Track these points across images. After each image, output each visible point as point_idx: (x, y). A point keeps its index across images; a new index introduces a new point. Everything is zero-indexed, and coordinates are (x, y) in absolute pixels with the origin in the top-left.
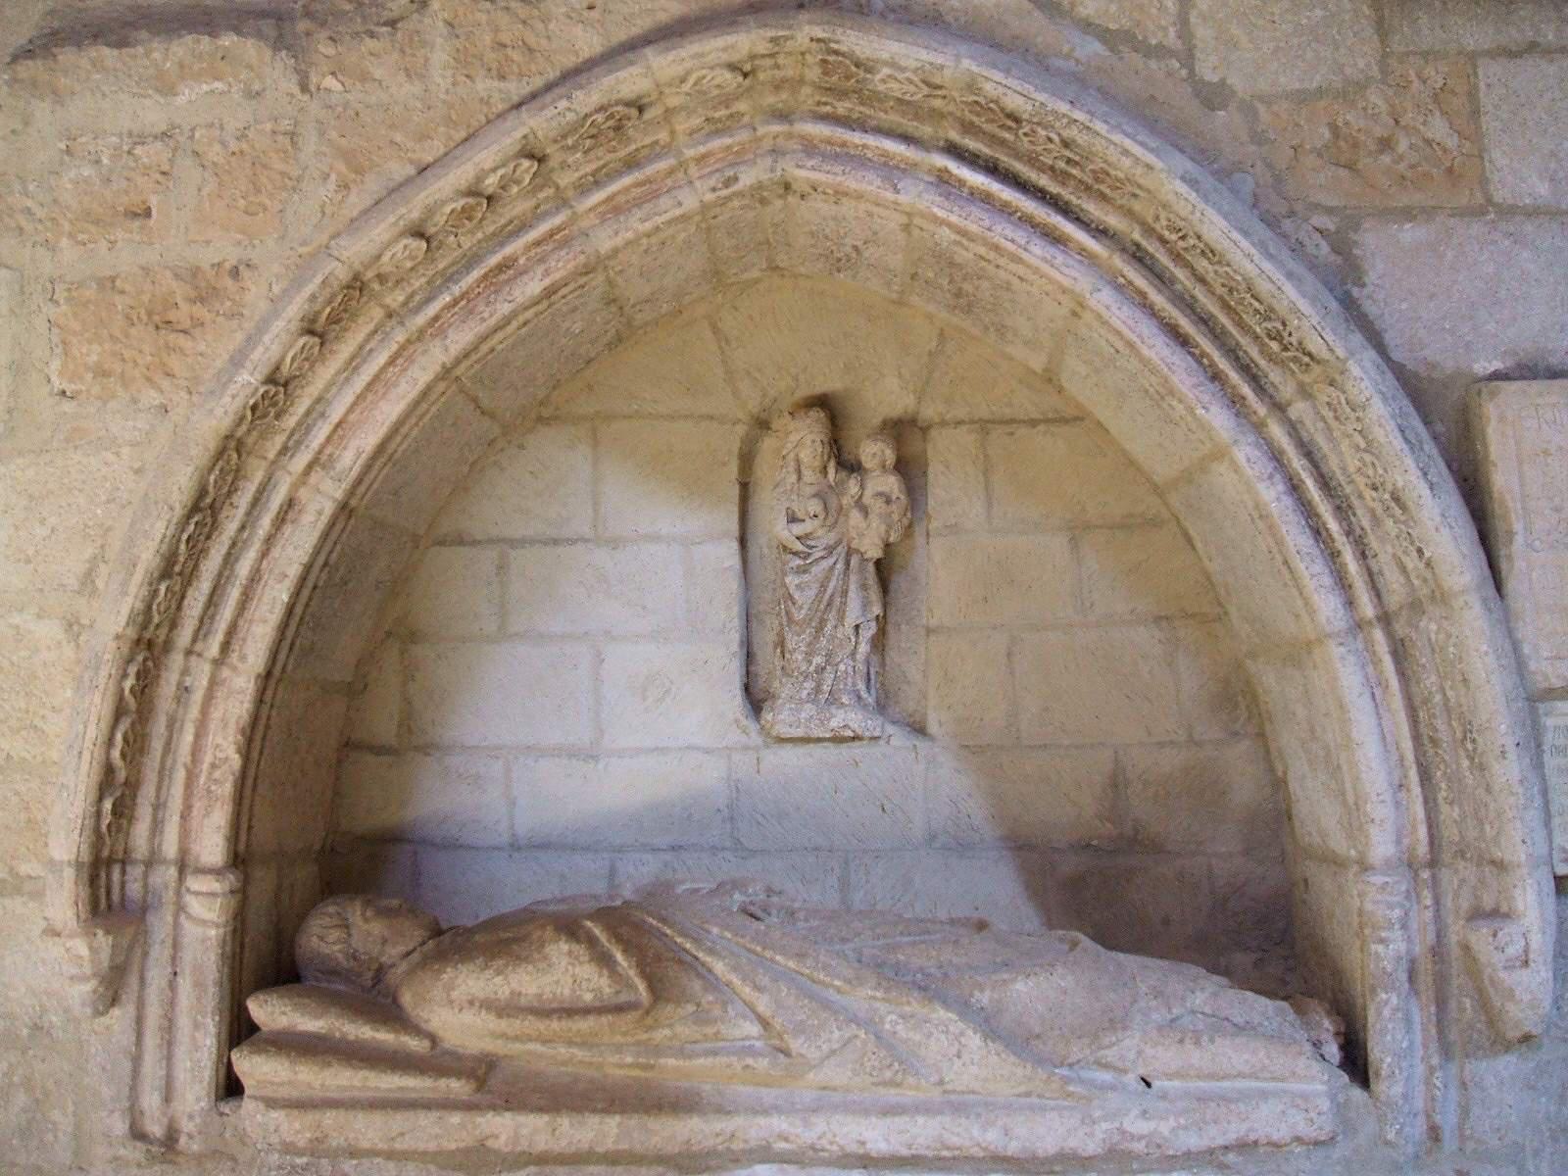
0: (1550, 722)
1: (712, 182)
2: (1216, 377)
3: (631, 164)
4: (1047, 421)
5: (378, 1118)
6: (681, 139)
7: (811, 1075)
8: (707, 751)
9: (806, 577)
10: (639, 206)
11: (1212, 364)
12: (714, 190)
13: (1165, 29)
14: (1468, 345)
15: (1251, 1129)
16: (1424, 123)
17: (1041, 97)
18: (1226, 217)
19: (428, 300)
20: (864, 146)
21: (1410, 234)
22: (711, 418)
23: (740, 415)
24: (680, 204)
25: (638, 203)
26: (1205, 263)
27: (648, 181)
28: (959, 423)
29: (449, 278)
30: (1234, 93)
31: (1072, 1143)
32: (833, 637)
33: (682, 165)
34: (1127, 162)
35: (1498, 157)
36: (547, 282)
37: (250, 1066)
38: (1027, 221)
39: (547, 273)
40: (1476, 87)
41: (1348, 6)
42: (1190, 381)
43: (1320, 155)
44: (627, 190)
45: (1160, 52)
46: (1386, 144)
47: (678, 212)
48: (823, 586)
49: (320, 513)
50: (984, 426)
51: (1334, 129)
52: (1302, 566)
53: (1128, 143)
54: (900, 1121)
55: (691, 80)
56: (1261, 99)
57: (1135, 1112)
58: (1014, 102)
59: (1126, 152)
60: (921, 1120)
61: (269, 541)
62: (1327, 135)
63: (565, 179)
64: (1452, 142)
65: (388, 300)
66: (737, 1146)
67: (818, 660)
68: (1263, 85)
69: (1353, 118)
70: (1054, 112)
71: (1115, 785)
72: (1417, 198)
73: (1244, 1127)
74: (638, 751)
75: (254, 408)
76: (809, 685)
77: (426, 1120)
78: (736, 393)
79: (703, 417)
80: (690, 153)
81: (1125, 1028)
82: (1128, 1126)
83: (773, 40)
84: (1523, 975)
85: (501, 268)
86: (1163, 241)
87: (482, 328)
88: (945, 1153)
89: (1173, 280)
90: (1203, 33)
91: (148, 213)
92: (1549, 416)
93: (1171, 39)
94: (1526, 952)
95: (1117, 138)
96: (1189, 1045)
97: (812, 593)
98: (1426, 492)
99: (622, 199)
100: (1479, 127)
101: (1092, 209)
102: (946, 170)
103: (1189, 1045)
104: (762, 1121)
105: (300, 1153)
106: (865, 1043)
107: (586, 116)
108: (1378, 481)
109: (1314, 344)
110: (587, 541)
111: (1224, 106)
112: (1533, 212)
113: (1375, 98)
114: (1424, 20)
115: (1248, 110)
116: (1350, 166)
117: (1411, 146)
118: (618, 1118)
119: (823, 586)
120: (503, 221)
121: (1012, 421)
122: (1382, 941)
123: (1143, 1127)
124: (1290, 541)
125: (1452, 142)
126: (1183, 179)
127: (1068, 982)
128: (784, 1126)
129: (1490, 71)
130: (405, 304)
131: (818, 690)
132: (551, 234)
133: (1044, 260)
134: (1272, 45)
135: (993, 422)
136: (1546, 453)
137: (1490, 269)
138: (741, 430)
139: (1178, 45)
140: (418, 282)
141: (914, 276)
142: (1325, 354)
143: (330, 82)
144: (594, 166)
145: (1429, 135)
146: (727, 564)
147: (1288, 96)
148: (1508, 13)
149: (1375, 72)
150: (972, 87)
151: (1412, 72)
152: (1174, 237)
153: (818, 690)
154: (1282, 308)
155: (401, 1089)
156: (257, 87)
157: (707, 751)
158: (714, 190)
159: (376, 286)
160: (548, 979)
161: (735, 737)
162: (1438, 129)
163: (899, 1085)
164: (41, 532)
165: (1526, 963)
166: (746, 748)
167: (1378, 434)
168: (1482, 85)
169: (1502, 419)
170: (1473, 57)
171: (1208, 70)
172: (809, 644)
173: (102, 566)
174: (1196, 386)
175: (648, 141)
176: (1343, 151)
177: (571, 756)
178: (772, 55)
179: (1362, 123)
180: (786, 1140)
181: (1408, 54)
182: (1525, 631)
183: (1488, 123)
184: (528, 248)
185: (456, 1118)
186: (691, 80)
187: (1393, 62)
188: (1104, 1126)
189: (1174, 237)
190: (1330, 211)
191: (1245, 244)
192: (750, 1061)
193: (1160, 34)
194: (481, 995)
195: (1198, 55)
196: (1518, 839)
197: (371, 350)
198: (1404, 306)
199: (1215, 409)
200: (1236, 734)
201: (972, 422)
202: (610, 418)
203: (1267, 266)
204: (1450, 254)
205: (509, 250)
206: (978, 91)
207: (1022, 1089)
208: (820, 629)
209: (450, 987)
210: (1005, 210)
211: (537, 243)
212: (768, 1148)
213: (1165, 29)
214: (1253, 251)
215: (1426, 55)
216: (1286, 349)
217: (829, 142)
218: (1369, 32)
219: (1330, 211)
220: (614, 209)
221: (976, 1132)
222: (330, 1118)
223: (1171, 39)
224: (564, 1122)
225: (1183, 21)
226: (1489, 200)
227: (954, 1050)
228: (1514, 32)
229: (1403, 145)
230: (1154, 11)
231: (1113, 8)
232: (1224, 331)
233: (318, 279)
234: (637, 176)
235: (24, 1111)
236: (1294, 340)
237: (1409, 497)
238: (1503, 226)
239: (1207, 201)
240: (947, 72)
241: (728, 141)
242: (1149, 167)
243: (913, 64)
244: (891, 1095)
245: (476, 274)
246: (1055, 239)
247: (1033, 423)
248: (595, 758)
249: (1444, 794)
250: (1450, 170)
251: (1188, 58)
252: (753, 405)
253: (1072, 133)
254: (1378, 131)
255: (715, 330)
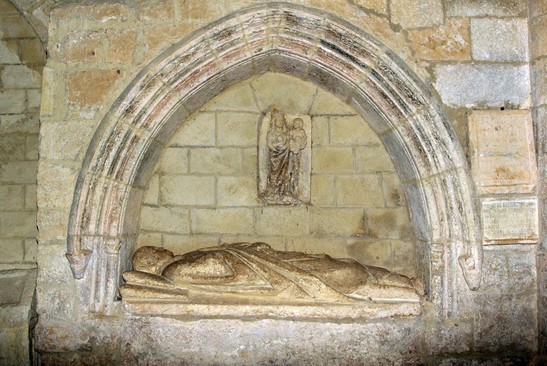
0: (484, 203)
1: (255, 50)
2: (394, 107)
3: (232, 44)
4: (347, 115)
5: (160, 306)
6: (247, 37)
7: (279, 295)
8: (248, 207)
9: (277, 159)
10: (235, 56)
11: (393, 103)
12: (255, 52)
13: (383, 9)
14: (465, 99)
15: (399, 311)
16: (455, 37)
17: (348, 30)
18: (398, 64)
19: (175, 81)
20: (298, 41)
21: (450, 68)
22: (250, 112)
23: (258, 111)
24: (246, 56)
25: (234, 55)
26: (392, 76)
27: (237, 49)
28: (322, 115)
29: (181, 75)
30: (402, 28)
31: (350, 314)
32: (284, 176)
33: (247, 44)
34: (370, 48)
35: (475, 47)
36: (209, 77)
37: (126, 292)
38: (343, 63)
39: (208, 74)
40: (470, 27)
41: (435, 3)
42: (386, 108)
43: (425, 45)
44: (231, 51)
45: (381, 15)
46: (444, 43)
47: (245, 58)
48: (282, 161)
49: (144, 140)
50: (329, 116)
51: (429, 38)
52: (416, 160)
53: (371, 43)
54: (304, 308)
55: (250, 22)
56: (409, 29)
57: (367, 306)
58: (340, 31)
59: (370, 46)
60: (309, 307)
61: (130, 147)
62: (427, 40)
63: (214, 47)
64: (463, 42)
65: (164, 81)
66: (258, 314)
67: (280, 182)
68: (410, 26)
69: (435, 35)
70: (351, 34)
71: (364, 219)
72: (453, 58)
73: (397, 311)
74: (227, 207)
75: (127, 110)
76: (277, 189)
77: (174, 306)
78: (257, 105)
79: (248, 112)
80: (249, 42)
81: (365, 284)
82: (365, 310)
83: (273, 11)
84: (474, 272)
85: (196, 72)
86: (380, 69)
87: (190, 89)
88: (315, 317)
89: (383, 80)
90: (393, 10)
91: (94, 53)
92: (485, 120)
93: (384, 12)
94: (474, 265)
95: (368, 42)
96: (382, 288)
97: (278, 163)
98: (450, 140)
99: (229, 54)
100: (470, 38)
101: (361, 59)
102: (321, 48)
103: (382, 288)
104: (266, 307)
105: (138, 315)
106: (294, 287)
107: (220, 32)
108: (438, 137)
109: (421, 99)
110: (213, 147)
111: (399, 31)
112: (485, 62)
113: (442, 30)
114: (456, 7)
115: (405, 33)
116: (434, 48)
117: (452, 43)
118: (226, 306)
119: (282, 161)
120: (196, 59)
121: (337, 115)
122: (436, 262)
123: (369, 310)
124: (413, 153)
125: (463, 42)
126: (386, 53)
127: (350, 271)
128: (272, 308)
129: (475, 22)
130: (168, 82)
131: (280, 190)
132: (209, 63)
133: (347, 74)
134: (413, 14)
135: (331, 115)
136: (484, 130)
137: (472, 78)
138: (259, 116)
139: (387, 14)
140: (172, 76)
141: (310, 74)
142: (424, 102)
143: (146, 18)
144: (221, 45)
145: (456, 40)
146: (254, 154)
147: (416, 29)
148: (480, 6)
149: (442, 22)
150: (328, 26)
151: (452, 22)
152: (383, 69)
153: (280, 190)
154: (412, 89)
155: (166, 298)
156: (125, 18)
157: (248, 207)
158: (255, 52)
159: (160, 77)
160: (207, 268)
161: (255, 204)
162: (459, 39)
163: (303, 298)
164: (64, 143)
165: (474, 268)
166: (258, 207)
167: (438, 124)
168: (472, 27)
169: (473, 121)
170: (470, 18)
171: (395, 21)
172: (278, 178)
173: (81, 153)
174: (388, 110)
175: (237, 37)
176: (433, 45)
177: (208, 208)
178: (273, 15)
179: (437, 37)
180: (272, 312)
181: (451, 17)
182: (476, 179)
183: (473, 37)
184: (203, 67)
185: (181, 306)
186: (250, 22)
187: (447, 19)
188: (359, 310)
189: (383, 69)
190: (427, 61)
191: (402, 72)
192: (262, 291)
193: (381, 10)
194: (189, 273)
195: (392, 17)
196: (473, 235)
197: (158, 95)
198: (447, 88)
199: (393, 116)
200: (399, 205)
201: (325, 115)
202: (221, 111)
203: (408, 78)
204: (460, 74)
205: (197, 68)
206: (330, 27)
207: (336, 300)
208: (280, 173)
209: (180, 271)
210: (337, 60)
211: (205, 66)
212: (267, 315)
213: (383, 9)
214: (405, 74)
215: (456, 17)
216: (413, 100)
217: (288, 39)
218: (441, 11)
219: (427, 61)
220: (227, 57)
221: (324, 311)
222: (146, 306)
223: (384, 12)
224: (212, 307)
225: (388, 5)
226: (472, 59)
227: (318, 289)
228: (481, 11)
229: (449, 43)
230: (380, 4)
231: (368, 3)
232: (397, 94)
233: (146, 76)
234: (234, 48)
235: (58, 304)
236: (416, 98)
237: (446, 141)
238: (476, 66)
239: (393, 60)
240: (322, 22)
241: (259, 38)
242: (377, 50)
243: (312, 20)
244: (301, 300)
245: (189, 74)
246: (350, 68)
247: (343, 116)
248: (215, 209)
249: (454, 222)
250: (462, 50)
251: (389, 18)
252: (262, 109)
253: (356, 40)
254: (442, 39)
255: (252, 87)
